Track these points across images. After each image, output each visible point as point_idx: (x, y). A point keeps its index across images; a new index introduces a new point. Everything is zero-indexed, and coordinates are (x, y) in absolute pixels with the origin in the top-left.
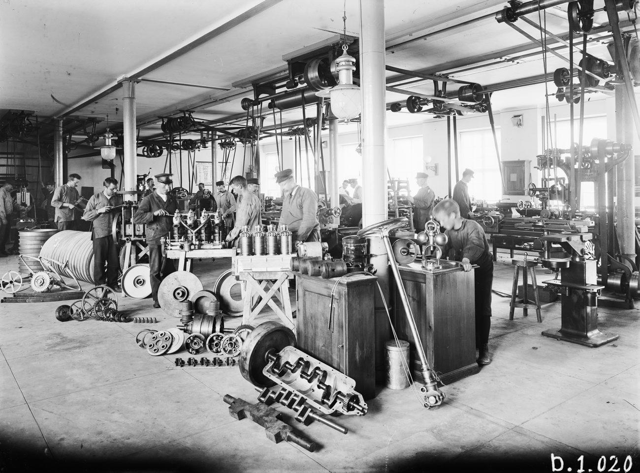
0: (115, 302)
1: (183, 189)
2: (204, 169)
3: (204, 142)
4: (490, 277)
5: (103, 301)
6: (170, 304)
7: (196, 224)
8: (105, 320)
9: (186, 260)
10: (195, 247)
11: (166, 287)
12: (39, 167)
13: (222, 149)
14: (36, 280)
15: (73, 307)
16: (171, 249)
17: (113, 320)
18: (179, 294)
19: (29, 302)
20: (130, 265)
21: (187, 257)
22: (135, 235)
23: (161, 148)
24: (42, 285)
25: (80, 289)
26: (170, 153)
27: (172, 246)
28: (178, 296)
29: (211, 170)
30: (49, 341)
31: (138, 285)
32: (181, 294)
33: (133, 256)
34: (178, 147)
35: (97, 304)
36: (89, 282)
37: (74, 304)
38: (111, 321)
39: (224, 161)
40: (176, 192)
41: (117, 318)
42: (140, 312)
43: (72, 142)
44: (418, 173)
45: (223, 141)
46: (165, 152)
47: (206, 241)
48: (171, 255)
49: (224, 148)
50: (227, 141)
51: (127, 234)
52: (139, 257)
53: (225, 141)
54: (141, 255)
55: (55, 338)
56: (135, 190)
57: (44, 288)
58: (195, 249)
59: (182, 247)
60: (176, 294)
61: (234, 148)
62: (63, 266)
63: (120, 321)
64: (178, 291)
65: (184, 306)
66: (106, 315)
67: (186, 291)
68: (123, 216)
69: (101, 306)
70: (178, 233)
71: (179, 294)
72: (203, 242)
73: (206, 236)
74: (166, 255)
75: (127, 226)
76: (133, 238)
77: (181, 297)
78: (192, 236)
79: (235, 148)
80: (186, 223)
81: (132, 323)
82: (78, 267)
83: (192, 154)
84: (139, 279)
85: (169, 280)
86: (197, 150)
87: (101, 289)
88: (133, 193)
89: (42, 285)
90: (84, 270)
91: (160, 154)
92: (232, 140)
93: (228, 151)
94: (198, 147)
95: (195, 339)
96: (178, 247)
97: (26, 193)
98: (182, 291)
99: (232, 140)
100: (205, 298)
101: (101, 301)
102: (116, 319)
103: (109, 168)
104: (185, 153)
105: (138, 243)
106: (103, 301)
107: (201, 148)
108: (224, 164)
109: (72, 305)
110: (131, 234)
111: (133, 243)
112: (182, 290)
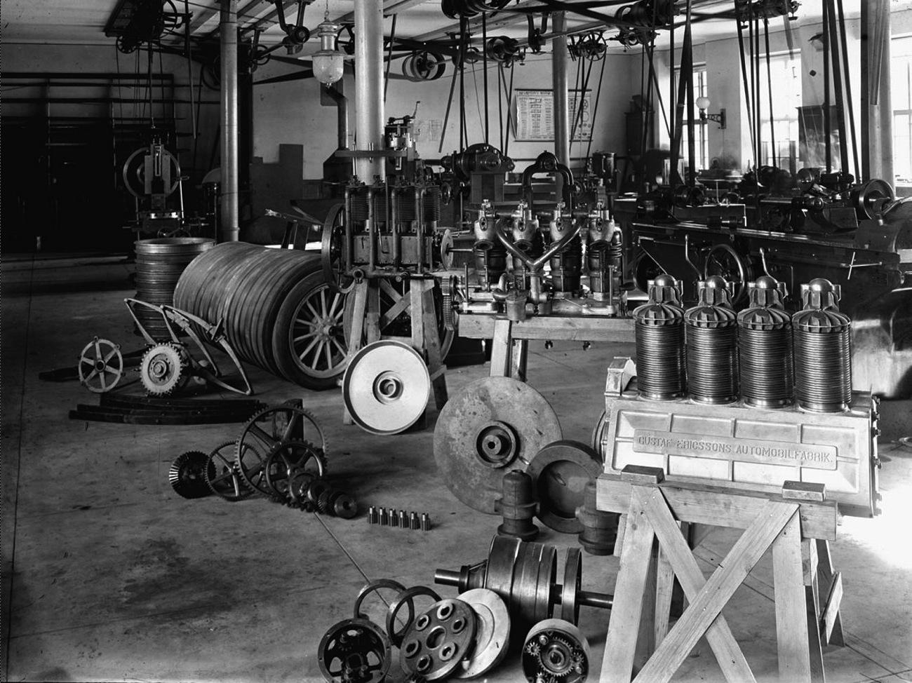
0: (319, 452)
1: (492, 149)
2: (532, 105)
3: (535, 40)
4: (360, 151)
5: (290, 450)
6: (467, 472)
7: (536, 245)
8: (294, 503)
9: (511, 342)
10: (536, 311)
11: (455, 419)
12: (191, 102)
13: (574, 59)
14: (152, 366)
15: (217, 461)
16: (470, 312)
17: (311, 507)
18: (492, 445)
19: (129, 423)
20: (364, 340)
21: (513, 336)
22: (376, 263)
23: (440, 59)
24: (163, 378)
25: (248, 392)
26: (462, 68)
27: (471, 302)
28: (493, 454)
29: (107, 266)
30: (138, 572)
31: (385, 397)
32: (498, 447)
33: (373, 317)
34: (474, 56)
35: (274, 457)
36: (267, 370)
37: (216, 451)
38: (309, 511)
39: (580, 87)
40: (475, 153)
41: (324, 503)
42: (387, 481)
43: (259, 48)
44: (546, 151)
45: (577, 39)
46: (450, 67)
47: (565, 291)
48: (468, 327)
49: (579, 56)
50: (587, 39)
51: (358, 259)
52: (387, 319)
53: (581, 40)
54: (393, 313)
55: (156, 559)
56: (381, 149)
57: (168, 386)
58: (535, 314)
59: (499, 307)
60: (485, 446)
61: (601, 55)
62: (213, 333)
63: (332, 514)
64: (490, 437)
65: (508, 493)
66: (295, 491)
67: (512, 437)
68: (347, 214)
69: (283, 463)
70: (489, 267)
71: (492, 445)
72: (560, 295)
73: (565, 277)
74: (456, 326)
75: (359, 238)
76: (371, 272)
77: (500, 453)
78: (528, 279)
79: (605, 55)
80: (510, 238)
81: (362, 523)
82: (247, 336)
83: (507, 72)
84: (387, 381)
85: (466, 400)
86: (517, 64)
87: (284, 414)
88: (373, 155)
89: (163, 378)
90: (261, 344)
91: (441, 70)
92: (596, 37)
93: (587, 62)
94: (521, 57)
95: (553, 643)
96: (488, 308)
97: (165, 157)
98: (500, 437)
99: (596, 37)
100: (567, 465)
101: (283, 449)
102: (321, 504)
103: (335, 105)
104: (493, 67)
105: (384, 283)
106: (290, 450)
107: (527, 57)
108: (579, 94)
109: (213, 454)
110: (365, 260)
111: (373, 283)
112: (500, 432)
